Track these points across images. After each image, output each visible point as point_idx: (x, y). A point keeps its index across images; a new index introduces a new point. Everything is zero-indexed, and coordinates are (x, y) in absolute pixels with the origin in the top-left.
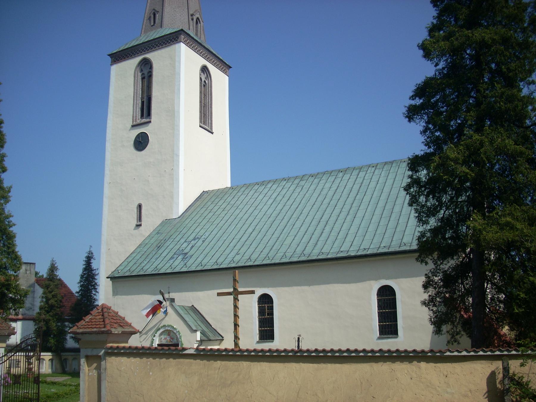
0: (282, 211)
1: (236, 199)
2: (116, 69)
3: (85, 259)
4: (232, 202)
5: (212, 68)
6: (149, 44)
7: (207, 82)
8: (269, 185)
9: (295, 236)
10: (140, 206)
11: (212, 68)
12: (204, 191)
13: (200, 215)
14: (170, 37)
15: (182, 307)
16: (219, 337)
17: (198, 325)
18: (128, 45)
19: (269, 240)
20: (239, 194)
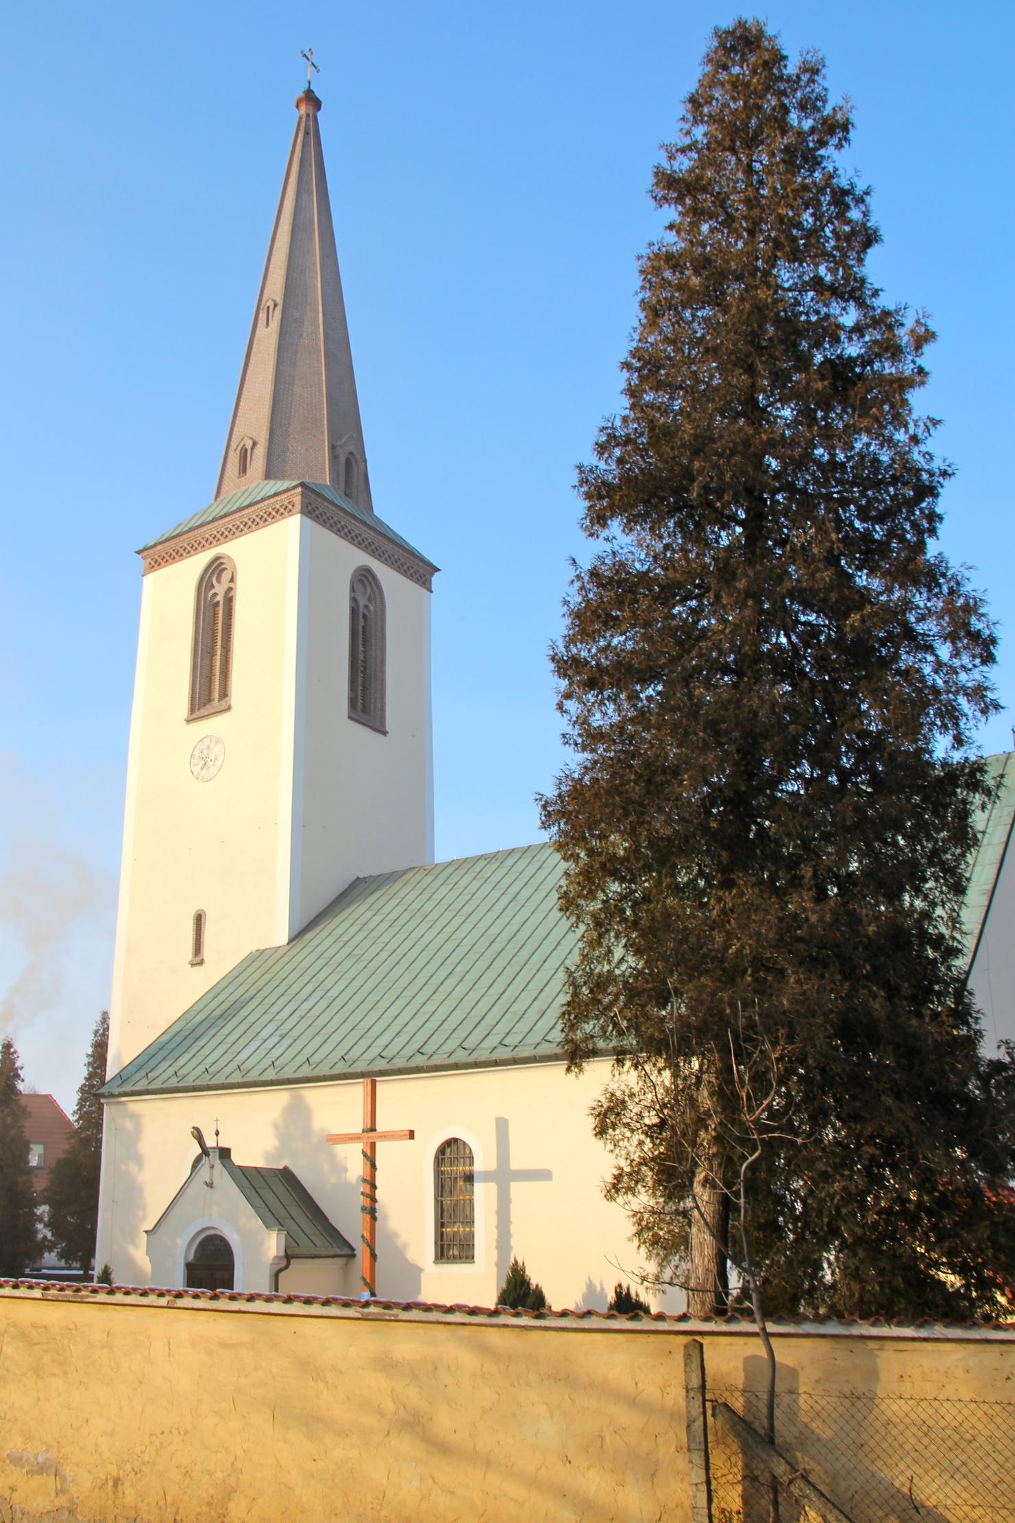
0: (438, 931)
1: (425, 896)
2: (152, 582)
3: (86, 1060)
4: (416, 905)
5: (383, 572)
6: (229, 522)
7: (372, 608)
8: (509, 862)
9: (542, 990)
10: (199, 919)
11: (383, 572)
12: (358, 878)
13: (372, 934)
14: (229, 522)
15: (238, 1170)
16: (341, 1250)
17: (288, 1216)
18: (229, 507)
19: (478, 1002)
20: (437, 884)
